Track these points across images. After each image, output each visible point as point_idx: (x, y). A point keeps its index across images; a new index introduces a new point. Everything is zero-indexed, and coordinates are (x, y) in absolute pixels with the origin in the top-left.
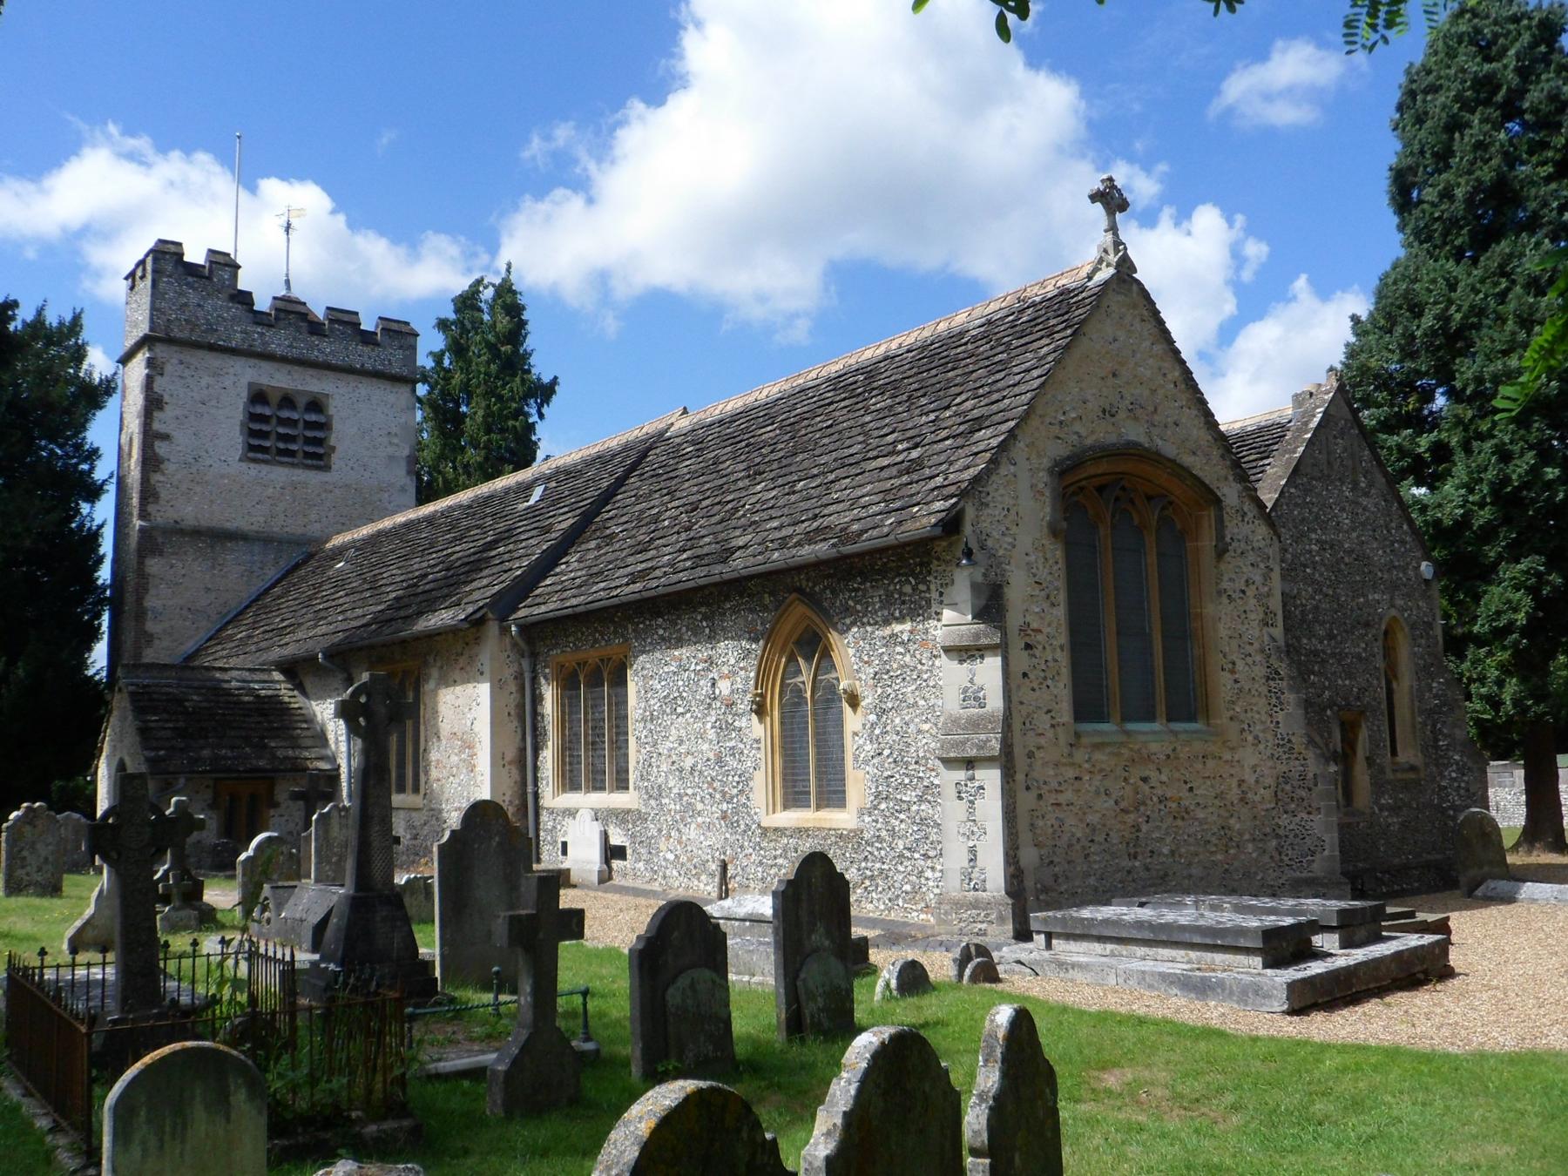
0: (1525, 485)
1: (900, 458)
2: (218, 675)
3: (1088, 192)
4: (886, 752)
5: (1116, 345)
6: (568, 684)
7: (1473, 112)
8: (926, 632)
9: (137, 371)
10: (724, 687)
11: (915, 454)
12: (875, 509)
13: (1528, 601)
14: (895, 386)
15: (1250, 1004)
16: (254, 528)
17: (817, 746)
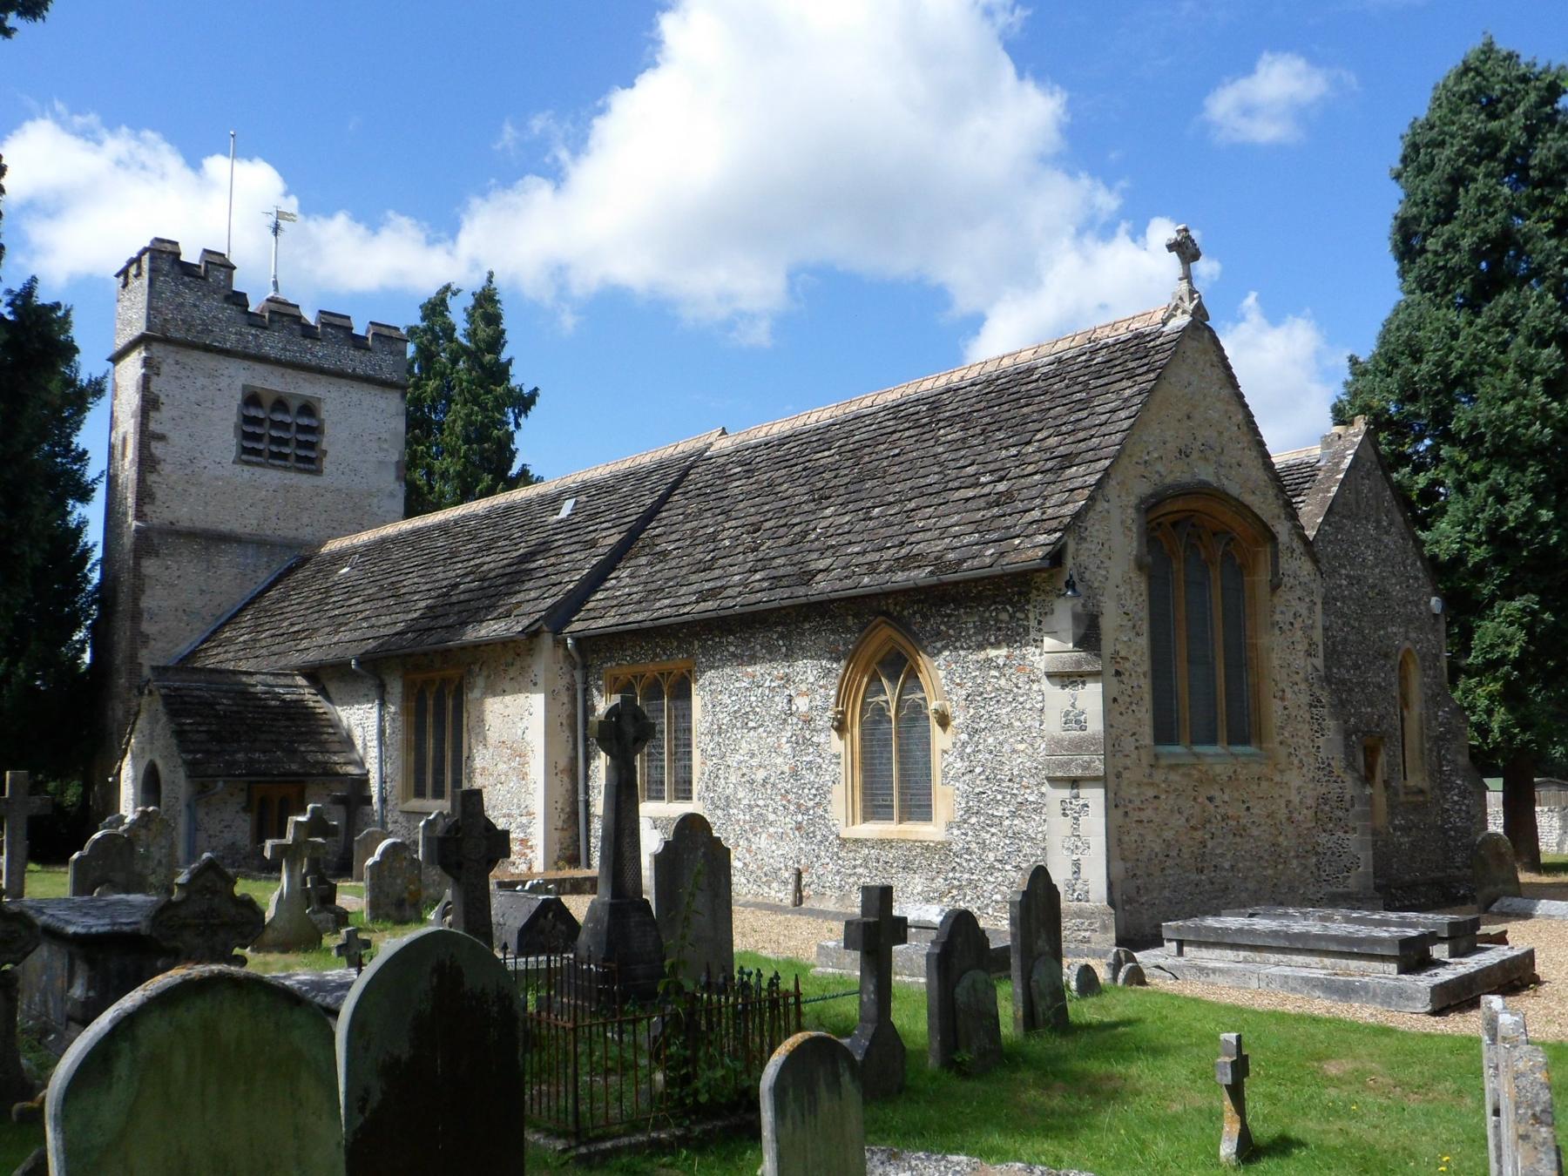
0: (1521, 527)
1: (986, 490)
2: (244, 679)
4: (978, 770)
5: (1191, 388)
7: (1477, 165)
8: (1024, 657)
9: (132, 369)
10: (802, 704)
11: (1001, 487)
12: (966, 540)
13: (1522, 636)
14: (966, 420)
15: (1397, 1005)
16: (247, 530)
17: (901, 763)
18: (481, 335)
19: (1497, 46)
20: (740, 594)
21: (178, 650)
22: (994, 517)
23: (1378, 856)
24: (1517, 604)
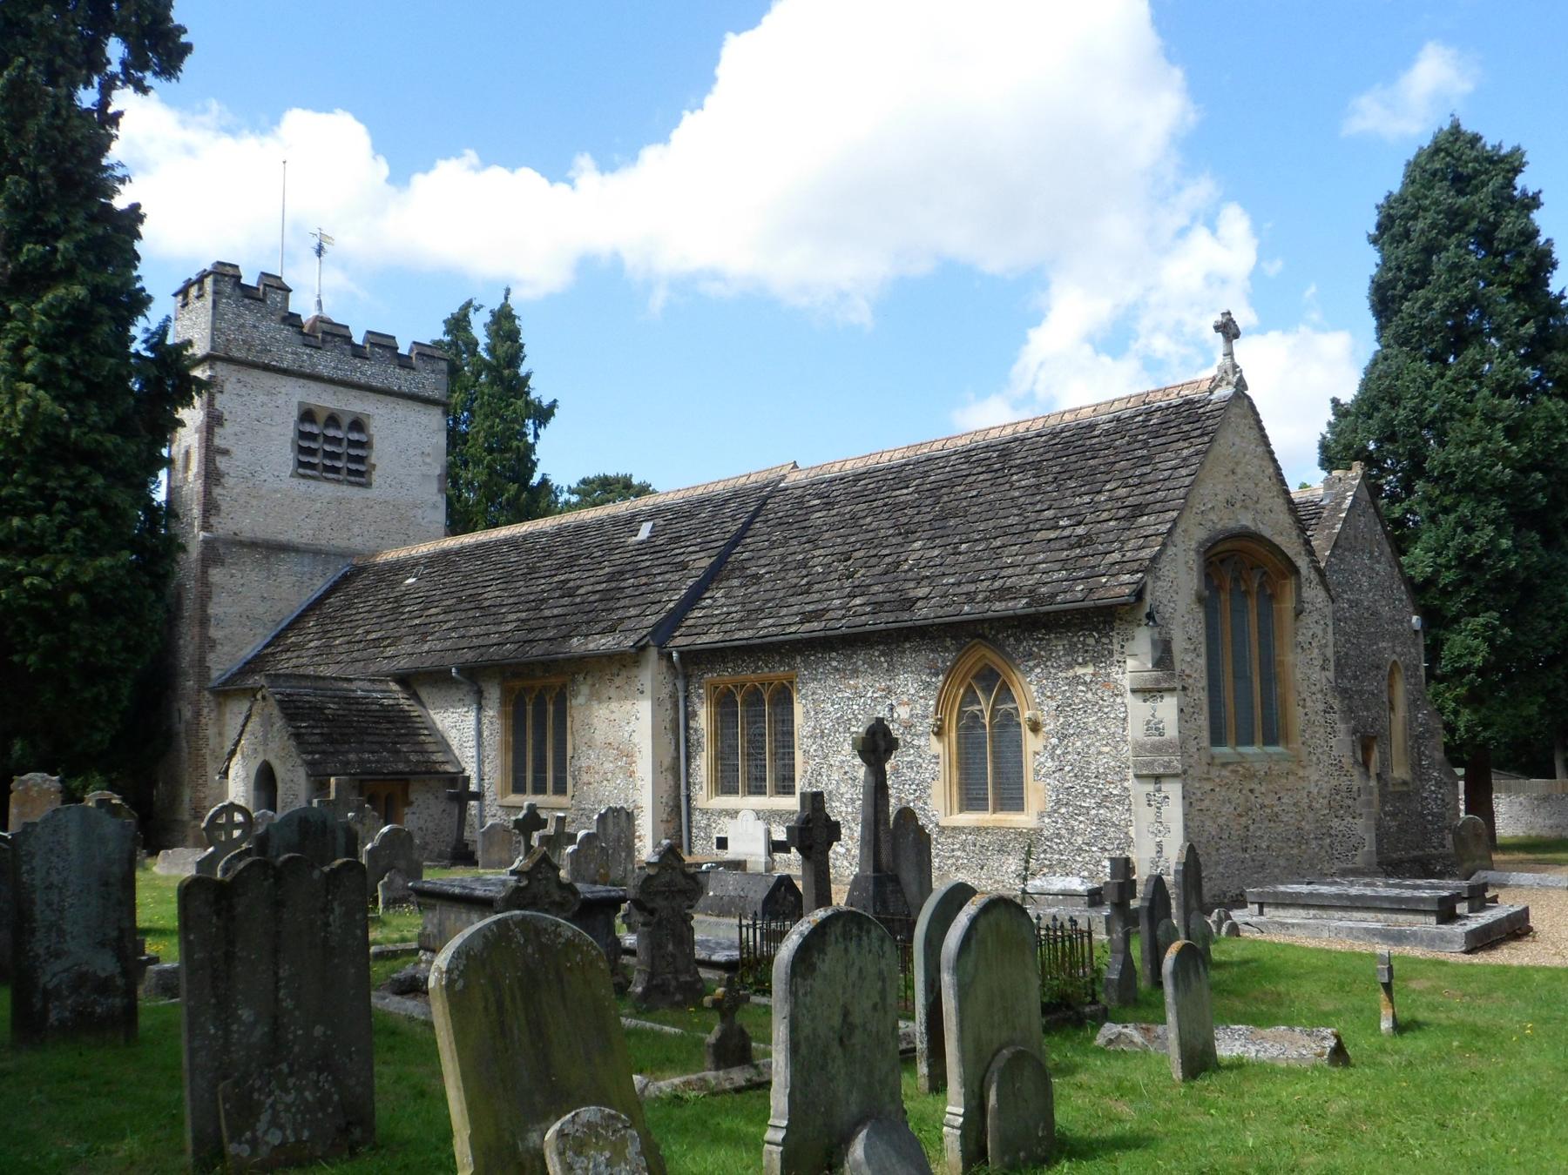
0: (1486, 554)
1: (1067, 533)
3: (1212, 324)
6: (724, 704)
7: (1448, 237)
11: (1080, 530)
13: (1484, 647)
14: (1037, 468)
15: (1432, 946)
17: (994, 762)
18: (500, 351)
19: (1464, 127)
20: (844, 617)
21: (243, 653)
22: (1078, 557)
23: (1379, 841)
24: (1481, 620)
